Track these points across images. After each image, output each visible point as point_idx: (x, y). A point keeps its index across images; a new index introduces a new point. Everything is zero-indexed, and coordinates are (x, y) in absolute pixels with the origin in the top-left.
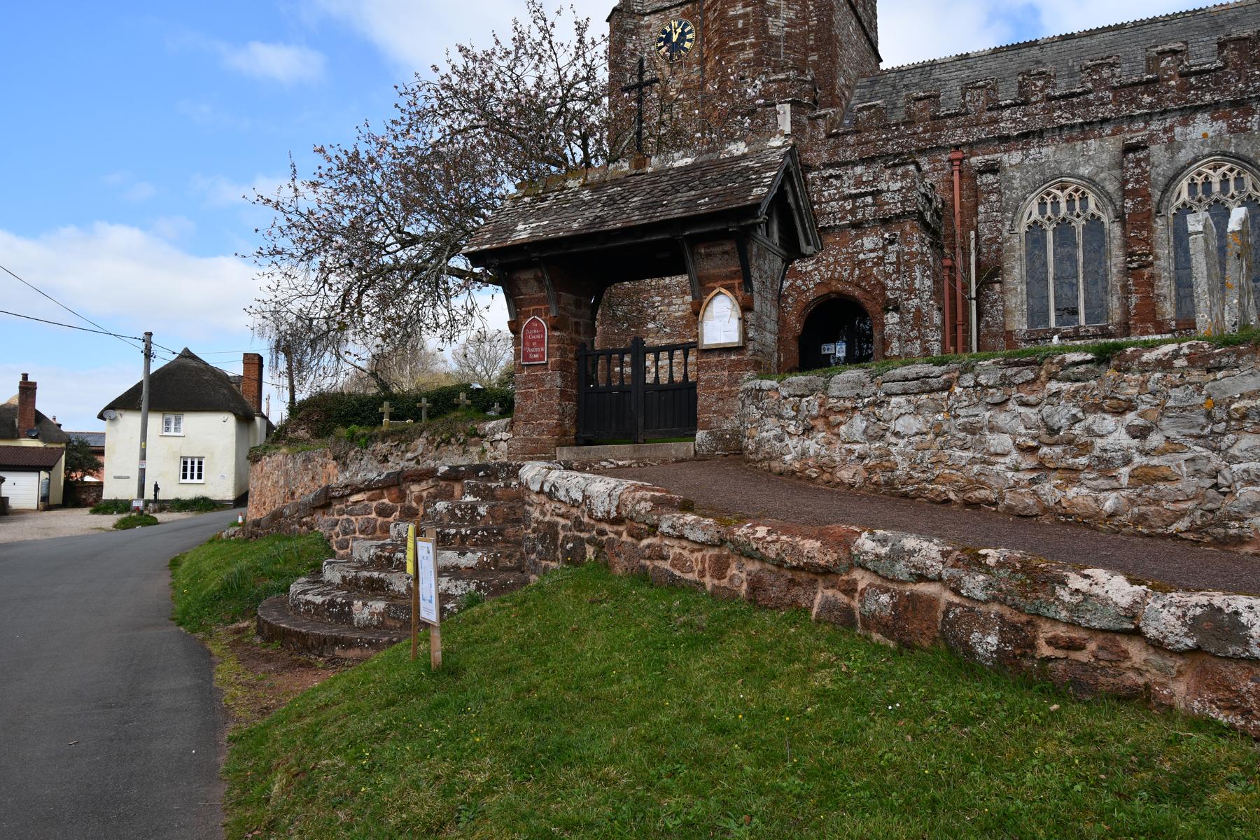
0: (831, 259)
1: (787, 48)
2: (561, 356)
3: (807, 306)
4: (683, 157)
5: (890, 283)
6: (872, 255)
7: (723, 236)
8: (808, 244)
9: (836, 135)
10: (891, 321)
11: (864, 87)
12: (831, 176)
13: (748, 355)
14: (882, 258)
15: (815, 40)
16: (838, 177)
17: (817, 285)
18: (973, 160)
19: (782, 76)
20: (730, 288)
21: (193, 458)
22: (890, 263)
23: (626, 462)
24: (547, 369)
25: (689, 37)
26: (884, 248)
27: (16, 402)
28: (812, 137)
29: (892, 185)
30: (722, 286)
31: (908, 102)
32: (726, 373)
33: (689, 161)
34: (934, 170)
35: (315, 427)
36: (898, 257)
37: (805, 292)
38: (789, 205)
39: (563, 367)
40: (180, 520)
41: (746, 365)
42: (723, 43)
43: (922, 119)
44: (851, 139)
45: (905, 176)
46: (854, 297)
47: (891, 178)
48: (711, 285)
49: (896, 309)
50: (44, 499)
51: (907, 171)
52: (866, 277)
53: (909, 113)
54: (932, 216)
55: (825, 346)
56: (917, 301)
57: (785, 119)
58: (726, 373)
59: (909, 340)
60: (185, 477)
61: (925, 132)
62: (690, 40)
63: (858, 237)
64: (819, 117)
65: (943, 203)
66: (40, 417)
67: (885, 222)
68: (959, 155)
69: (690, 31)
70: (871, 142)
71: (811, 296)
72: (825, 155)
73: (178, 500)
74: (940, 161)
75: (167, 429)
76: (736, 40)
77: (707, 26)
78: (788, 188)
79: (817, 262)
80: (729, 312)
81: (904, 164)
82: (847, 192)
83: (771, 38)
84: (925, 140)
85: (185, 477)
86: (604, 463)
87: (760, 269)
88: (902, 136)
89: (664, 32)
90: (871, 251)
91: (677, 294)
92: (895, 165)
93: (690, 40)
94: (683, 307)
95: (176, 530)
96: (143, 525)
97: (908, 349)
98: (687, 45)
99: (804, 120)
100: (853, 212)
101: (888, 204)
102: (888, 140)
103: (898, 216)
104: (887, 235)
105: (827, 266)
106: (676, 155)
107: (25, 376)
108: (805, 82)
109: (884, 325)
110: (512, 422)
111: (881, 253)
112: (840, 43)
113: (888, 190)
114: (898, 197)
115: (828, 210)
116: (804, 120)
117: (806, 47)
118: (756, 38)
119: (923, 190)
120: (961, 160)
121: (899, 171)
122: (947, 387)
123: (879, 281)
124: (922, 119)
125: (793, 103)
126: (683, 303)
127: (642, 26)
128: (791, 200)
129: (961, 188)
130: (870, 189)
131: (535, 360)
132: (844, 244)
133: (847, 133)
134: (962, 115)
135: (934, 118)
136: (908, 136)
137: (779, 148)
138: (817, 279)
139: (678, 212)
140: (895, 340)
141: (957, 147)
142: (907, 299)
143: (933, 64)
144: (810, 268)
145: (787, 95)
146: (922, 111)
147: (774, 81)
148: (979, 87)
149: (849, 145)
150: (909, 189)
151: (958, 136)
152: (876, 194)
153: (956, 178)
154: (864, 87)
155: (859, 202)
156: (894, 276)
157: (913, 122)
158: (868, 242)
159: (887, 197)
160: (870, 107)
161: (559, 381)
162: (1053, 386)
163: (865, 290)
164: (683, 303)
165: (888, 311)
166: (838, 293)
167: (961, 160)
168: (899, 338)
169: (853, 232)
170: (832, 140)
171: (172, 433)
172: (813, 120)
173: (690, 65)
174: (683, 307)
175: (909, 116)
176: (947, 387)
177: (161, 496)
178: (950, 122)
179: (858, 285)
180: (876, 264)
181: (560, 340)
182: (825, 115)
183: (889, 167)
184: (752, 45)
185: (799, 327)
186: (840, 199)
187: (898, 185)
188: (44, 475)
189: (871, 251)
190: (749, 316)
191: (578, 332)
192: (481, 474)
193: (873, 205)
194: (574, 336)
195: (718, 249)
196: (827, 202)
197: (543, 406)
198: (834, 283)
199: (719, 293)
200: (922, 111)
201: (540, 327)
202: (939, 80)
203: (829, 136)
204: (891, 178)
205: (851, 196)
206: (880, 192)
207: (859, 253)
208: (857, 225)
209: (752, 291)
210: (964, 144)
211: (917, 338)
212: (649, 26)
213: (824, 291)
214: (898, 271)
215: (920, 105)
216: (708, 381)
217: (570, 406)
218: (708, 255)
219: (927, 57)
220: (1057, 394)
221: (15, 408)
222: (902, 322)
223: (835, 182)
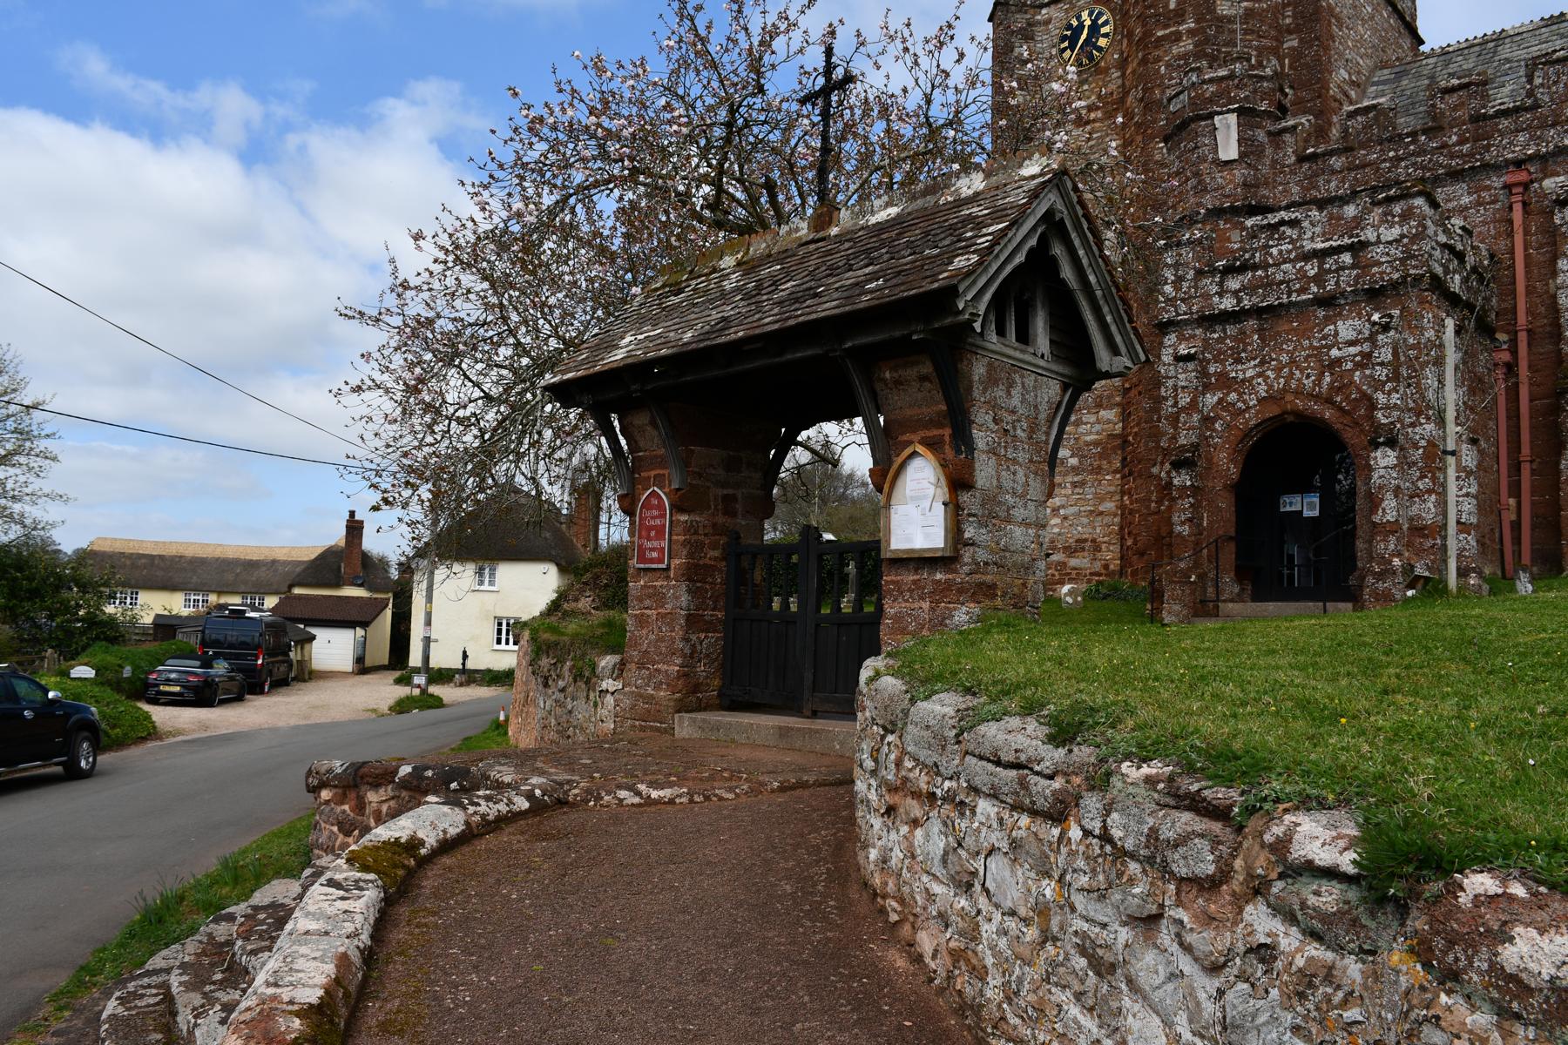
0: (1284, 358)
1: (1246, 32)
2: (690, 555)
3: (1247, 434)
4: (888, 205)
5: (1381, 398)
6: (1353, 350)
7: (901, 351)
8: (1115, 351)
9: (1314, 156)
10: (1382, 463)
11: (1384, 83)
12: (1282, 223)
13: (961, 575)
14: (1368, 356)
15: (1294, 17)
16: (1294, 223)
17: (1261, 401)
18: (1548, 183)
19: (1222, 73)
20: (933, 445)
21: (508, 619)
22: (1382, 364)
23: (666, 793)
24: (668, 578)
25: (1104, 30)
26: (1372, 339)
27: (342, 543)
28: (1274, 162)
29: (1384, 233)
30: (924, 442)
31: (1433, 97)
32: (926, 605)
33: (893, 211)
34: (1479, 203)
35: (603, 594)
36: (1395, 354)
37: (1241, 412)
38: (1063, 282)
39: (694, 574)
40: (480, 700)
41: (961, 591)
42: (1147, 34)
43: (1455, 123)
44: (1337, 162)
45: (1406, 216)
46: (1323, 420)
47: (1382, 222)
48: (906, 437)
49: (1391, 443)
50: (360, 660)
51: (1411, 208)
52: (1342, 387)
53: (1433, 113)
54: (1465, 280)
55: (1286, 499)
56: (1430, 427)
57: (1228, 137)
58: (926, 605)
59: (1416, 494)
60: (499, 642)
61: (1461, 142)
62: (1106, 35)
63: (1329, 320)
64: (1285, 130)
65: (1492, 256)
66: (366, 558)
67: (1374, 295)
68: (1522, 176)
69: (1106, 23)
70: (1369, 164)
71: (1252, 419)
72: (1295, 189)
73: (489, 671)
74: (1488, 188)
75: (481, 583)
76: (1166, 27)
77: (1127, 12)
78: (1058, 250)
79: (1262, 363)
80: (931, 490)
81: (1405, 196)
82: (1308, 246)
83: (1221, 19)
84: (1462, 156)
85: (499, 642)
86: (623, 794)
87: (993, 405)
88: (1422, 152)
89: (1069, 27)
90: (1351, 343)
91: (1088, 408)
92: (1389, 200)
93: (1106, 35)
94: (1098, 427)
95: (463, 718)
96: (421, 708)
97: (1414, 511)
98: (1102, 42)
99: (1261, 135)
100: (1319, 279)
101: (1379, 264)
102: (1399, 159)
103: (1395, 285)
104: (1376, 317)
105: (1278, 370)
106: (877, 203)
107: (352, 514)
108: (1262, 78)
109: (1370, 469)
110: (623, 663)
111: (1366, 347)
112: (1338, 19)
113: (1379, 242)
114: (1396, 252)
115: (1279, 277)
116: (1261, 135)
117: (1279, 28)
118: (1197, 21)
119: (1442, 238)
120: (1526, 186)
121: (1397, 209)
122: (1058, 813)
123: (1364, 395)
124: (1455, 123)
125: (1241, 112)
126: (1098, 421)
127: (1039, 23)
128: (1067, 273)
129: (1526, 232)
130: (1347, 241)
131: (652, 561)
132: (1304, 333)
133: (1331, 153)
134: (1527, 109)
135: (1477, 119)
136: (1434, 151)
137: (1033, 177)
138: (1262, 390)
139: (828, 307)
140: (1389, 495)
141: (1519, 164)
142: (1413, 425)
143: (1500, 38)
144: (1249, 373)
145: (1231, 101)
146: (1455, 108)
147: (1211, 81)
148: (1558, 61)
149: (1334, 172)
150: (1420, 236)
151: (1521, 145)
152: (1358, 248)
153: (1517, 215)
154: (1384, 83)
155: (1329, 263)
156: (1388, 386)
157: (1441, 128)
158: (1346, 329)
159: (1377, 252)
160: (1367, 109)
161: (684, 599)
162: (1260, 921)
163: (1341, 409)
164: (1098, 421)
165: (1377, 446)
166: (1297, 414)
167: (1526, 186)
168: (1397, 491)
169: (1321, 313)
170: (1306, 166)
171: (486, 587)
172: (1275, 136)
173: (1106, 71)
174: (1098, 427)
175: (1434, 119)
176: (1058, 813)
177: (470, 665)
178: (1504, 123)
179: (1329, 401)
180: (1358, 366)
181: (690, 529)
182: (1295, 127)
183: (1379, 203)
184: (1191, 32)
185: (1234, 471)
186: (1297, 259)
187: (1396, 232)
188: (360, 632)
189: (1351, 343)
190: (965, 497)
191: (730, 512)
192: (454, 785)
193: (1353, 267)
194: (721, 519)
195: (911, 373)
196: (1277, 265)
197: (661, 639)
198: (1289, 397)
199: (914, 454)
200: (1455, 108)
201: (661, 506)
202: (1508, 60)
203: (1302, 159)
204: (1382, 222)
205: (1321, 255)
206: (1364, 245)
207: (1330, 347)
208: (1327, 302)
209: (971, 448)
210: (1530, 158)
211: (1430, 492)
212: (1048, 22)
213: (1272, 411)
214: (1395, 377)
215: (1453, 99)
216: (898, 618)
217: (710, 641)
218: (898, 383)
219: (1490, 27)
220: (1265, 953)
221: (342, 551)
222: (1403, 464)
223: (1289, 232)
